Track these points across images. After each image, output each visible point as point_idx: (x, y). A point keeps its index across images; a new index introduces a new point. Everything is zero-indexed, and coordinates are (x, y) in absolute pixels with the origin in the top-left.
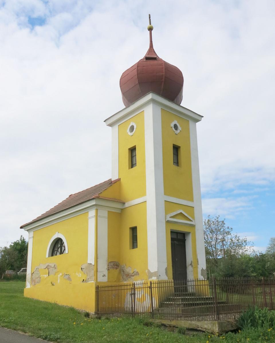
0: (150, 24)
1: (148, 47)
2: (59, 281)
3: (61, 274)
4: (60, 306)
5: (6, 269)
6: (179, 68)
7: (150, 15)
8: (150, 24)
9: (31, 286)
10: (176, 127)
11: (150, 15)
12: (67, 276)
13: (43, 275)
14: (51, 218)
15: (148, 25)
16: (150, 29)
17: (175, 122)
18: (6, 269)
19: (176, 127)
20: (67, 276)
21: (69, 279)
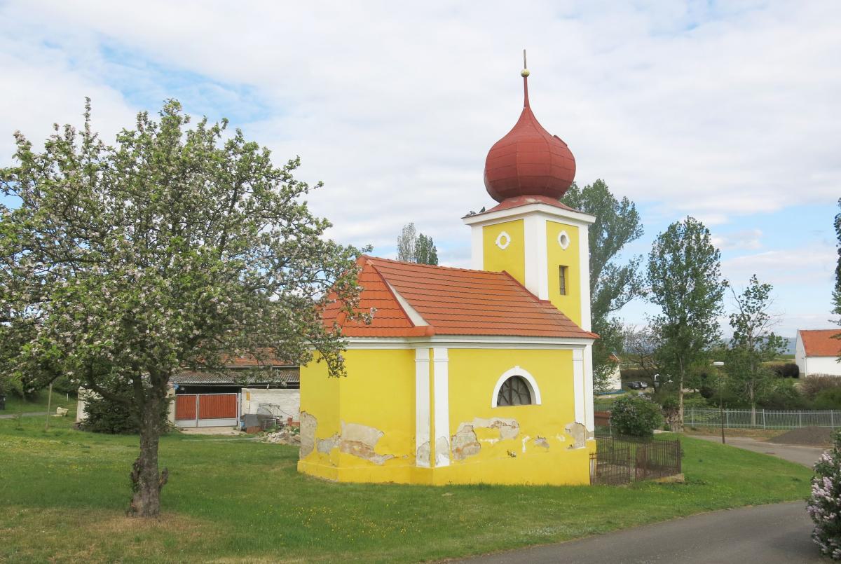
0: (525, 67)
1: (521, 107)
2: (524, 449)
3: (528, 437)
4: (576, 487)
5: (797, 385)
6: (571, 151)
7: (525, 51)
8: (525, 67)
9: (453, 462)
10: (563, 238)
11: (525, 51)
12: (541, 441)
13: (484, 439)
14: (35, 411)
15: (521, 69)
16: (525, 76)
17: (563, 233)
18: (797, 385)
19: (563, 238)
20: (541, 441)
21: (545, 444)
